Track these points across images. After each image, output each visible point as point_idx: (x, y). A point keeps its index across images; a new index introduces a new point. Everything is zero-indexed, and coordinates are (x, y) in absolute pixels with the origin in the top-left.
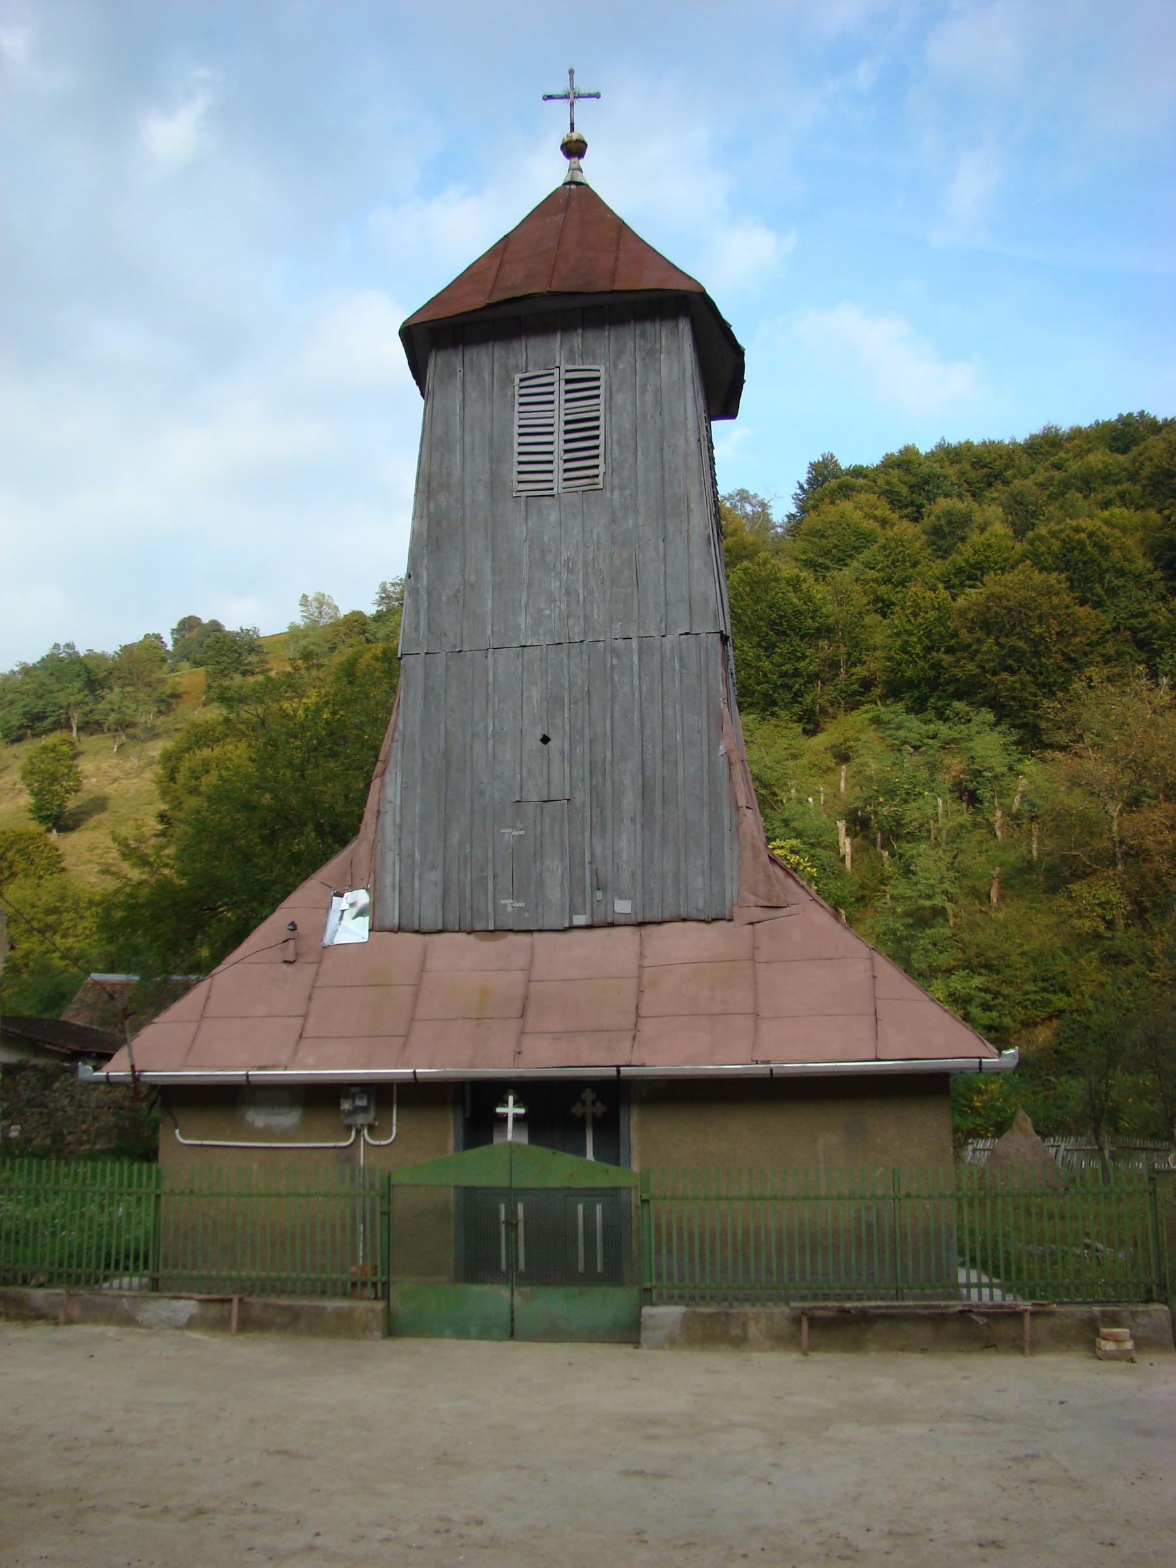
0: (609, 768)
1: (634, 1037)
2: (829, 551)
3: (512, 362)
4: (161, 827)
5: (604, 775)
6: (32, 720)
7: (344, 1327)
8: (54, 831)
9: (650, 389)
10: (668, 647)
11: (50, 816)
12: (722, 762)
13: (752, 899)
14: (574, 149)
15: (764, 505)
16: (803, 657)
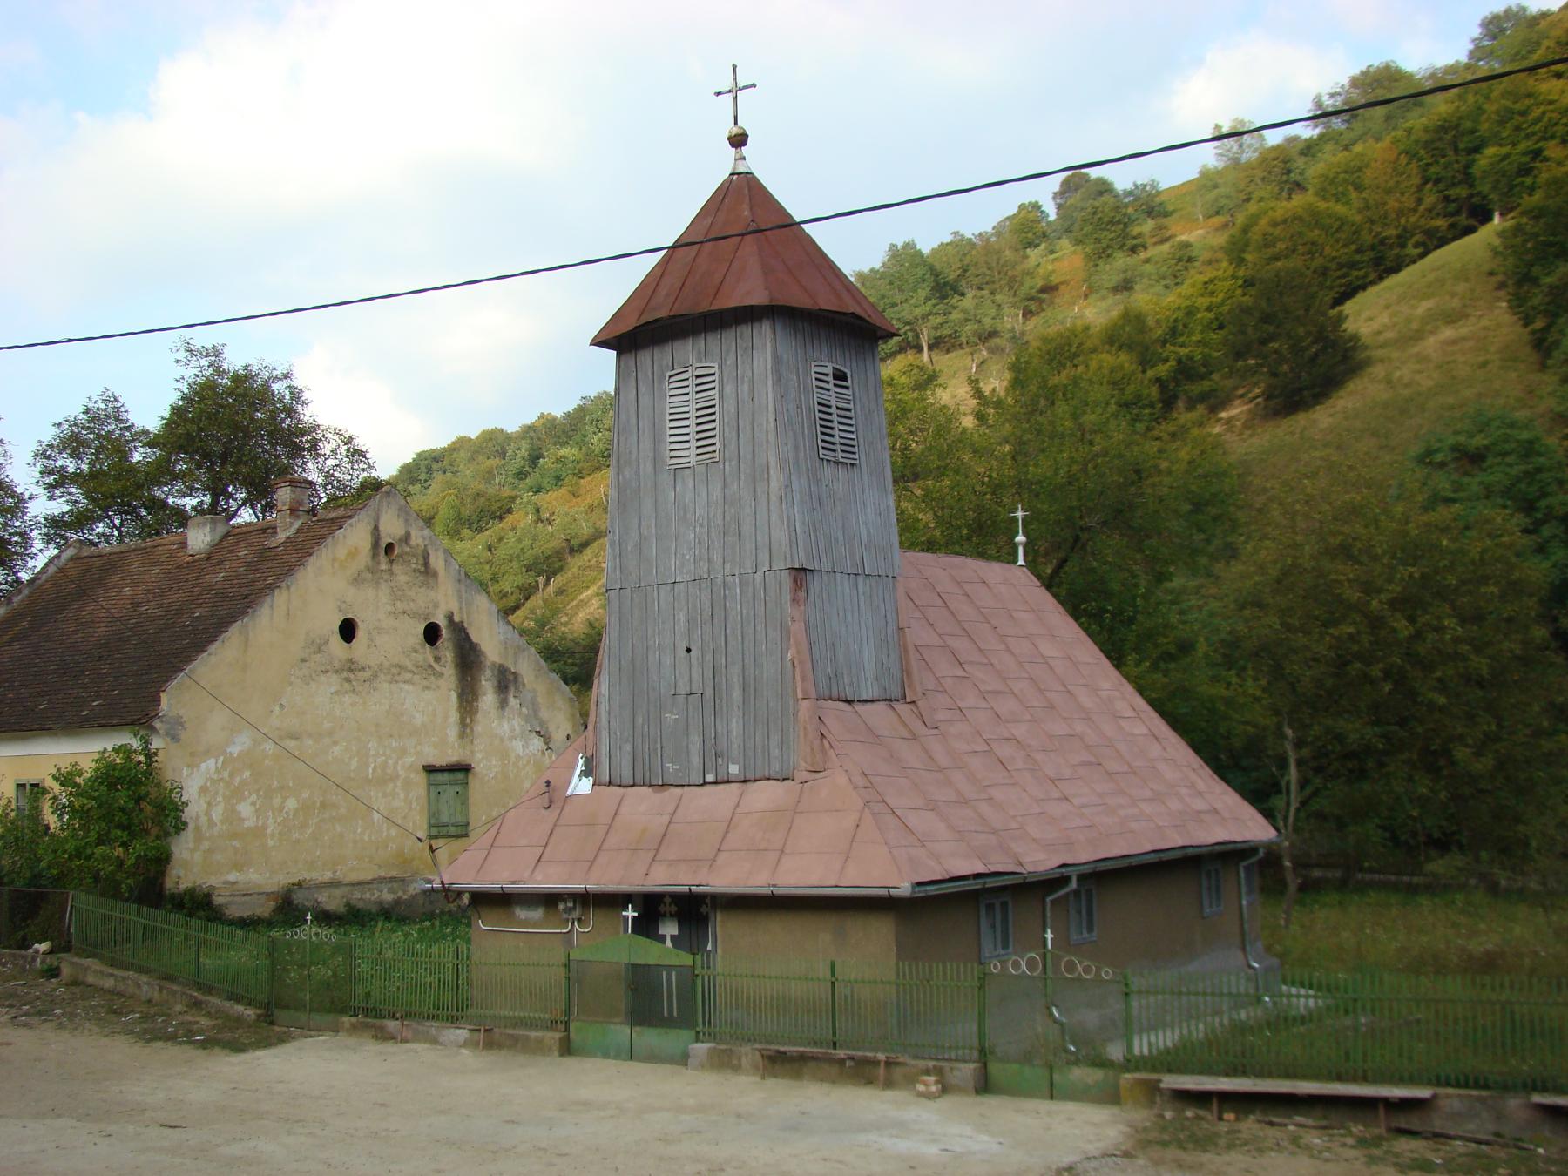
7: (538, 1049)
12: (789, 665)
14: (738, 141)
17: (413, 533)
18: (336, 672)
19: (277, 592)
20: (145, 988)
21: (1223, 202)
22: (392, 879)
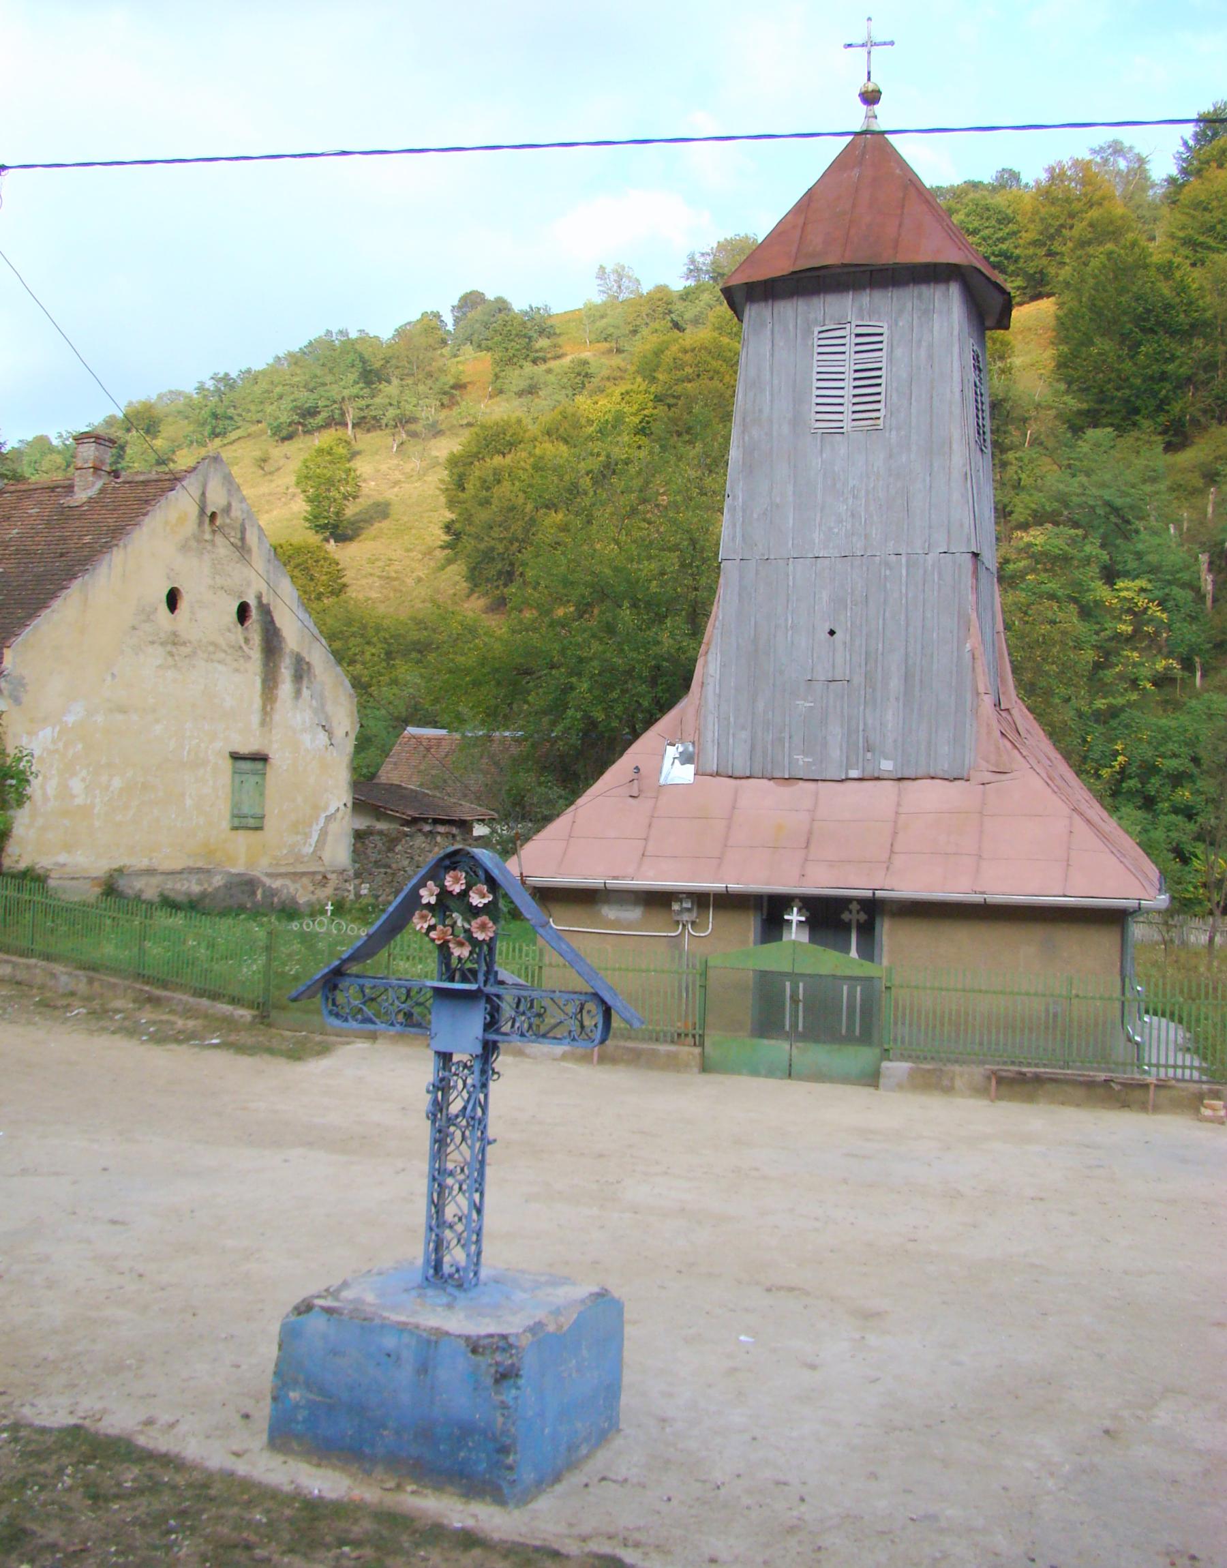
0: (880, 657)
1: (888, 868)
2: (1213, 228)
3: (812, 316)
4: (447, 538)
5: (876, 661)
6: (303, 416)
7: (672, 1064)
8: (332, 541)
9: (924, 344)
10: (930, 562)
11: (326, 525)
12: (968, 656)
13: (984, 764)
14: (870, 98)
15: (1141, 161)
16: (1173, 358)
17: (233, 504)
18: (162, 644)
19: (115, 549)
20: (64, 979)
21: (611, 330)
22: (200, 870)
